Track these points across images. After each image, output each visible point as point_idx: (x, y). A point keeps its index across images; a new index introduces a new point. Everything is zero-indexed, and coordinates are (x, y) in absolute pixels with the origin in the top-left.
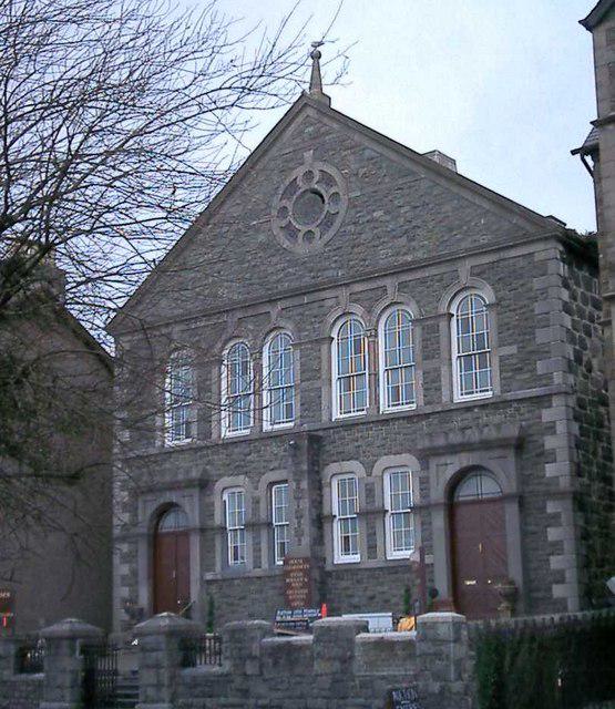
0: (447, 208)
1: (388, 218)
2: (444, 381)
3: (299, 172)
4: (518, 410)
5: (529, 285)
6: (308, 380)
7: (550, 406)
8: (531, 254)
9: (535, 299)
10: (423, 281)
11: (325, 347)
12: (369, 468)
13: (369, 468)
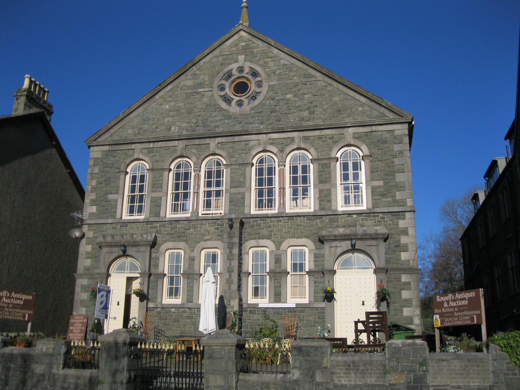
0: (336, 99)
1: (296, 99)
2: (119, 208)
3: (234, 66)
4: (383, 218)
5: (391, 147)
6: (235, 187)
7: (404, 218)
8: (393, 131)
9: (395, 157)
10: (320, 138)
11: (166, 173)
12: (278, 245)
13: (278, 245)
